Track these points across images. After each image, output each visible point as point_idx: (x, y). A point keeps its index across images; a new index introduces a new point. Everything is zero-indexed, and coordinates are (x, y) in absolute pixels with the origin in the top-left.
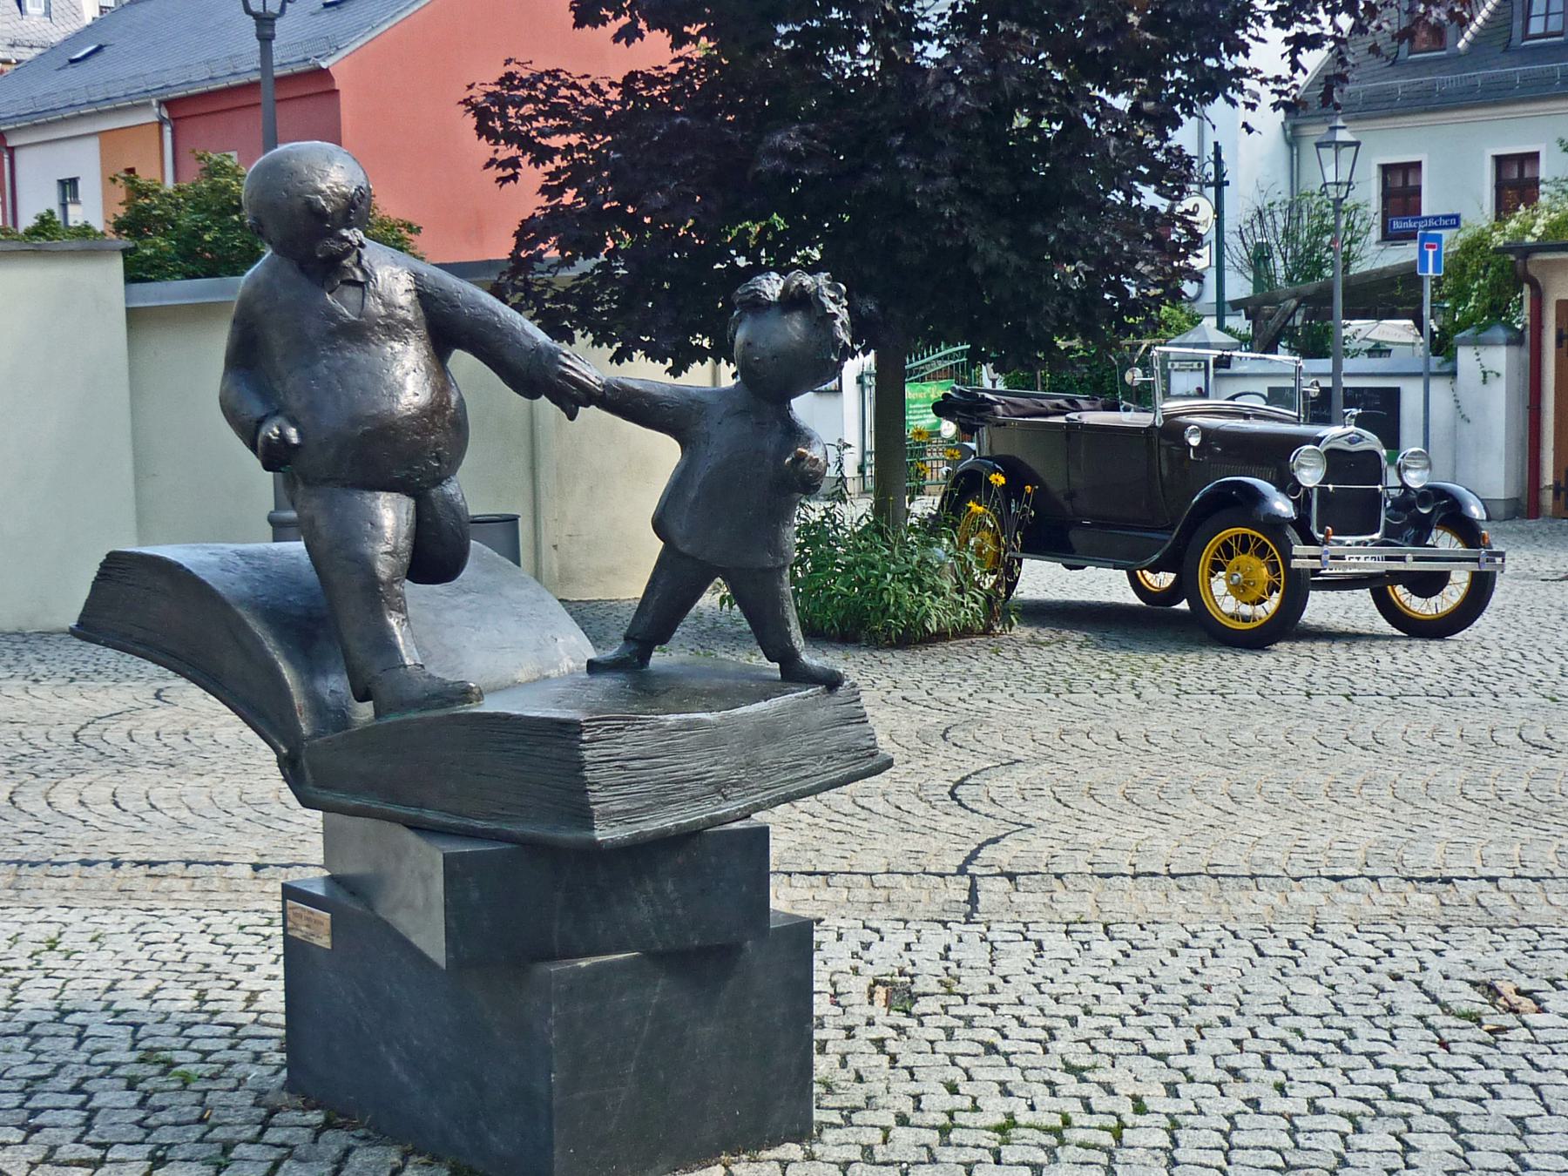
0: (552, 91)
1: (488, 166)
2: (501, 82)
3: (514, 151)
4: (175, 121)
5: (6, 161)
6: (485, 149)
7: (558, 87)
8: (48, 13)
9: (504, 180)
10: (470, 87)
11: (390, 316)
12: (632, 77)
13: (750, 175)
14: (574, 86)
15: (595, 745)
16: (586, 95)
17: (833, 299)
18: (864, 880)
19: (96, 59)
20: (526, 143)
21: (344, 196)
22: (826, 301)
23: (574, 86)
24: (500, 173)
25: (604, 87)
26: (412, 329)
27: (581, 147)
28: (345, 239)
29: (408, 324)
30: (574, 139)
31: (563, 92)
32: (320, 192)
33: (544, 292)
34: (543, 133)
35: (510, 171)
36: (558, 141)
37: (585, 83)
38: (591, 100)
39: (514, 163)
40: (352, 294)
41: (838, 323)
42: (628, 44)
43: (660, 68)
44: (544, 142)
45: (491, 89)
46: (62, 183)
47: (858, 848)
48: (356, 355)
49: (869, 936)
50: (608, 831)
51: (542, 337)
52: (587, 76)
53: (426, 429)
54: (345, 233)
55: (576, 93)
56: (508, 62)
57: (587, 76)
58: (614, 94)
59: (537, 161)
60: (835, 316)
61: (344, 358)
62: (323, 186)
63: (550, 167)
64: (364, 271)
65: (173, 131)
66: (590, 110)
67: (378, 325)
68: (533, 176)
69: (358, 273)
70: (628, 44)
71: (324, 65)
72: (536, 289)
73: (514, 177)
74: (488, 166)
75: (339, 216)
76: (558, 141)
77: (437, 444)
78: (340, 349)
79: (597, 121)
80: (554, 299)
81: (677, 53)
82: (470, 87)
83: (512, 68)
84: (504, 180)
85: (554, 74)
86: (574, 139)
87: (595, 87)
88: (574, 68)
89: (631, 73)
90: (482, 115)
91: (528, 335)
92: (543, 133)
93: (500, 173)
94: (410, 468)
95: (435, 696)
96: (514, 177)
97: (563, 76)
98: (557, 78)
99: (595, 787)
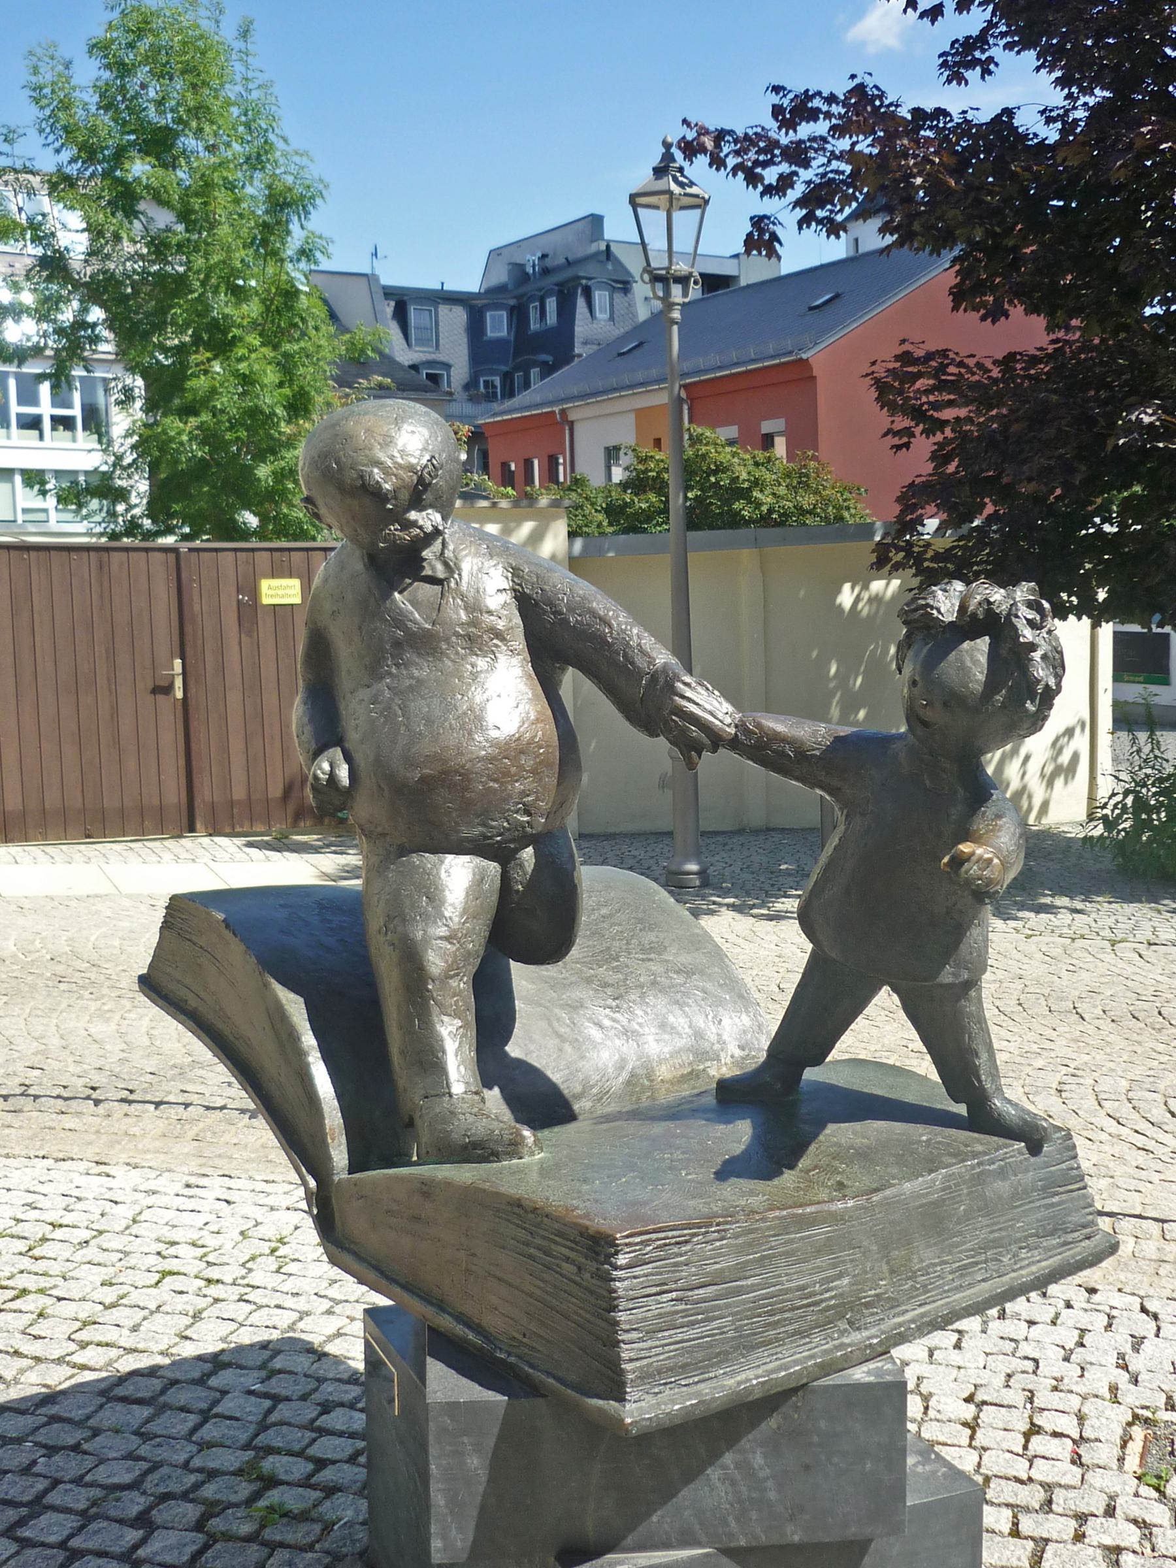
0: (942, 368)
1: (885, 435)
2: (897, 358)
3: (907, 423)
4: (692, 400)
5: (567, 432)
6: (883, 419)
7: (948, 365)
8: (612, 318)
9: (898, 447)
10: (874, 363)
11: (474, 623)
12: (1011, 357)
13: (1109, 448)
14: (961, 364)
15: (638, 1271)
16: (973, 374)
17: (1031, 623)
18: (1155, 1228)
19: (637, 352)
20: (918, 414)
21: (411, 468)
22: (1021, 624)
23: (961, 364)
24: (896, 441)
25: (988, 364)
26: (503, 639)
27: (969, 420)
28: (414, 524)
29: (499, 635)
30: (963, 412)
31: (952, 369)
32: (378, 463)
33: (925, 552)
34: (937, 406)
35: (905, 440)
36: (948, 414)
37: (971, 362)
38: (976, 378)
39: (908, 432)
40: (425, 591)
41: (1037, 655)
42: (994, 322)
43: (1041, 349)
44: (935, 414)
45: (891, 366)
46: (608, 450)
47: (1156, 1178)
48: (422, 670)
49: (1147, 1327)
50: (651, 1400)
51: (663, 657)
52: (973, 356)
53: (507, 774)
54: (413, 515)
55: (963, 370)
56: (903, 341)
57: (973, 356)
58: (996, 373)
59: (927, 432)
60: (1032, 647)
61: (412, 677)
62: (382, 457)
63: (939, 437)
64: (446, 564)
65: (690, 409)
66: (978, 385)
67: (458, 635)
68: (924, 446)
69: (439, 567)
70: (994, 322)
71: (804, 356)
72: (916, 549)
73: (907, 445)
74: (885, 435)
75: (405, 496)
76: (948, 414)
77: (524, 794)
78: (406, 665)
79: (983, 396)
80: (932, 559)
81: (1052, 337)
82: (874, 363)
83: (907, 347)
84: (898, 447)
85: (944, 353)
86: (963, 412)
87: (979, 365)
88: (960, 347)
89: (1010, 353)
90: (882, 388)
91: (643, 652)
92: (937, 406)
93: (896, 441)
94: (484, 825)
95: (475, 1145)
96: (907, 445)
97: (951, 355)
98: (947, 357)
99: (634, 1335)
